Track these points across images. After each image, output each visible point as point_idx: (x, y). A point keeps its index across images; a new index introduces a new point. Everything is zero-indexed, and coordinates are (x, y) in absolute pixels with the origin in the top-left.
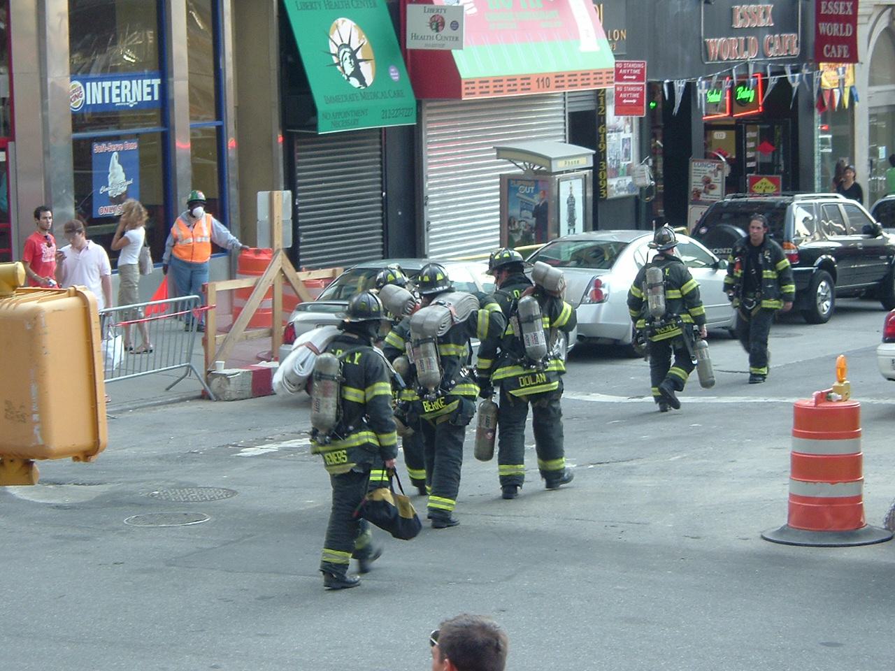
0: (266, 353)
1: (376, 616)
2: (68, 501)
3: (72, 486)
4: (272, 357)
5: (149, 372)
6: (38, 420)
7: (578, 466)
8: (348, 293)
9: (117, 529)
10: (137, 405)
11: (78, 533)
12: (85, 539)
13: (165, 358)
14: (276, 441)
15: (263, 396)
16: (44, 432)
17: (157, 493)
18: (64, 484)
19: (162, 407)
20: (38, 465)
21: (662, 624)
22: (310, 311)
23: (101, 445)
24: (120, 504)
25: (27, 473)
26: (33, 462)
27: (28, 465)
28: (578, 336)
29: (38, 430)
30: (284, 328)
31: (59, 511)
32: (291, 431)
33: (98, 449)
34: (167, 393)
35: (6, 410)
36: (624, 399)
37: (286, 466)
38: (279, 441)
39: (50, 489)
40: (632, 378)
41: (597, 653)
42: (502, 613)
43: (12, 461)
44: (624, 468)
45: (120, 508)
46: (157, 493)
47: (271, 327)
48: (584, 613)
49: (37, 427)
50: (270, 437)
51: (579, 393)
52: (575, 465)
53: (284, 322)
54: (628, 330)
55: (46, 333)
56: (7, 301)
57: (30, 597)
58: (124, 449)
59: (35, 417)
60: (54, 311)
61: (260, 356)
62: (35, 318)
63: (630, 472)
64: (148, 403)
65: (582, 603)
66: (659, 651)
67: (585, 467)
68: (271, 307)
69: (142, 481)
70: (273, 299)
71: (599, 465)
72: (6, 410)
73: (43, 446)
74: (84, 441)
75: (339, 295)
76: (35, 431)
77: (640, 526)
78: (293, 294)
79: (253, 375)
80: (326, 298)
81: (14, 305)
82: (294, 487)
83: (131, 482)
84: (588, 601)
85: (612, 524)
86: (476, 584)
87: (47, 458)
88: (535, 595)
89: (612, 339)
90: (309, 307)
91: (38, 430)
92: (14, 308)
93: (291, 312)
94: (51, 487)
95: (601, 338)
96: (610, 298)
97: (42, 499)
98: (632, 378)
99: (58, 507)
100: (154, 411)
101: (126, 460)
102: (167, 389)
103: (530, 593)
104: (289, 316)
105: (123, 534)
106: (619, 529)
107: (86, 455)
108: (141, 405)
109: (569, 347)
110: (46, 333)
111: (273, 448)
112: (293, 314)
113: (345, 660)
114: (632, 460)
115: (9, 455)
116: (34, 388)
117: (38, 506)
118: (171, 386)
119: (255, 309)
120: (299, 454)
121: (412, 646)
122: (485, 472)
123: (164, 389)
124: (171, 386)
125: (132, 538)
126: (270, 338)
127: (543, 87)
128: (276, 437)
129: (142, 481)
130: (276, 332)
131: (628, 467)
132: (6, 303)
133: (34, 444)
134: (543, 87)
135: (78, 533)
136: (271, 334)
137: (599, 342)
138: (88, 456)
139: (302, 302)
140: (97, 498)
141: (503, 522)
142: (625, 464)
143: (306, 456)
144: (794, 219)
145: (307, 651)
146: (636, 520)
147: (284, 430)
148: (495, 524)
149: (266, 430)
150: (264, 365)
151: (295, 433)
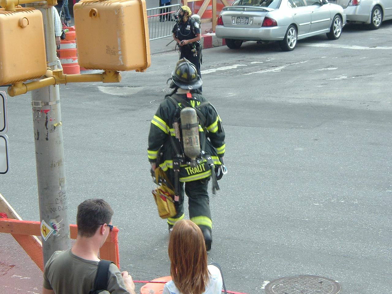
0: (209, 29)
1: (261, 142)
2: (125, 94)
3: (127, 87)
4: (212, 31)
5: (159, 38)
6: (121, 54)
7: (348, 77)
8: (245, 3)
9: (147, 106)
10: (154, 53)
11: (130, 107)
12: (133, 110)
13: (165, 32)
14: (215, 68)
15: (209, 48)
16: (124, 59)
17: (164, 90)
18: (123, 87)
19: (164, 53)
20: (121, 73)
21: (386, 145)
22: (228, 11)
23: (148, 65)
24: (148, 95)
25: (116, 77)
26: (119, 72)
27: (117, 74)
28: (347, 20)
29: (121, 58)
30: (217, 18)
31: (122, 98)
32: (221, 63)
33: (147, 67)
34: (167, 47)
35: (107, 50)
36: (367, 48)
37: (219, 78)
38: (216, 68)
39: (118, 89)
40: (371, 39)
41: (358, 158)
42: (316, 141)
43: (109, 72)
44: (368, 78)
45: (149, 97)
46: (164, 90)
47: (212, 18)
48: (352, 141)
49: (120, 57)
50: (212, 66)
51: (348, 45)
52: (347, 77)
53: (217, 16)
54: (369, 17)
55: (123, 16)
56: (107, 2)
57: (111, 135)
58: (149, 71)
59: (120, 53)
60: (127, 6)
61: (207, 30)
62: (119, 10)
63: (371, 79)
64: (158, 52)
65: (351, 136)
66: (385, 157)
67: (351, 78)
68: (211, 9)
69: (158, 85)
70: (212, 6)
71: (357, 77)
72: (107, 50)
73: (123, 65)
74: (141, 63)
75: (241, 4)
76: (120, 59)
77: (376, 103)
78: (221, 3)
79: (204, 39)
80: (236, 5)
81: (109, 4)
82: (223, 87)
83: (153, 86)
84: (354, 135)
85: (364, 102)
86: (304, 128)
87: (125, 70)
88: (330, 133)
89: (362, 22)
90: (228, 9)
91: (121, 58)
92: (110, 5)
93: (220, 11)
94: (118, 88)
95: (357, 21)
96: (361, 4)
97: (115, 93)
98: (371, 39)
99: (121, 97)
100: (161, 55)
101: (150, 76)
102: (167, 46)
103: (328, 133)
104: (219, 14)
105: (149, 108)
106: (367, 104)
107: (142, 69)
108: (156, 52)
109: (343, 25)
110: (123, 16)
111: (214, 70)
112: (221, 12)
113: (248, 161)
114: (372, 74)
115: (108, 69)
116: (119, 40)
117: (113, 96)
118: (168, 45)
119: (204, 10)
120: (225, 73)
121: (277, 155)
122: (307, 80)
123: (165, 46)
124: (168, 45)
125: (154, 109)
126: (211, 23)
127: (167, 20)
128: (215, 66)
129: (158, 85)
130: (214, 20)
131: (370, 78)
132: (106, 3)
133: (119, 64)
134: (167, 20)
135: (130, 107)
136: (212, 21)
137: (356, 23)
138: (142, 70)
139: (225, 6)
140: (138, 92)
141: (315, 102)
142: (369, 76)
143: (228, 74)
144: (161, 114)
145: (231, 157)
146: (374, 101)
147: (218, 63)
148: (311, 102)
149: (210, 63)
150: (209, 34)
151: (223, 64)
